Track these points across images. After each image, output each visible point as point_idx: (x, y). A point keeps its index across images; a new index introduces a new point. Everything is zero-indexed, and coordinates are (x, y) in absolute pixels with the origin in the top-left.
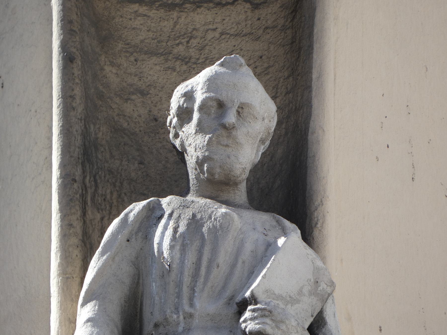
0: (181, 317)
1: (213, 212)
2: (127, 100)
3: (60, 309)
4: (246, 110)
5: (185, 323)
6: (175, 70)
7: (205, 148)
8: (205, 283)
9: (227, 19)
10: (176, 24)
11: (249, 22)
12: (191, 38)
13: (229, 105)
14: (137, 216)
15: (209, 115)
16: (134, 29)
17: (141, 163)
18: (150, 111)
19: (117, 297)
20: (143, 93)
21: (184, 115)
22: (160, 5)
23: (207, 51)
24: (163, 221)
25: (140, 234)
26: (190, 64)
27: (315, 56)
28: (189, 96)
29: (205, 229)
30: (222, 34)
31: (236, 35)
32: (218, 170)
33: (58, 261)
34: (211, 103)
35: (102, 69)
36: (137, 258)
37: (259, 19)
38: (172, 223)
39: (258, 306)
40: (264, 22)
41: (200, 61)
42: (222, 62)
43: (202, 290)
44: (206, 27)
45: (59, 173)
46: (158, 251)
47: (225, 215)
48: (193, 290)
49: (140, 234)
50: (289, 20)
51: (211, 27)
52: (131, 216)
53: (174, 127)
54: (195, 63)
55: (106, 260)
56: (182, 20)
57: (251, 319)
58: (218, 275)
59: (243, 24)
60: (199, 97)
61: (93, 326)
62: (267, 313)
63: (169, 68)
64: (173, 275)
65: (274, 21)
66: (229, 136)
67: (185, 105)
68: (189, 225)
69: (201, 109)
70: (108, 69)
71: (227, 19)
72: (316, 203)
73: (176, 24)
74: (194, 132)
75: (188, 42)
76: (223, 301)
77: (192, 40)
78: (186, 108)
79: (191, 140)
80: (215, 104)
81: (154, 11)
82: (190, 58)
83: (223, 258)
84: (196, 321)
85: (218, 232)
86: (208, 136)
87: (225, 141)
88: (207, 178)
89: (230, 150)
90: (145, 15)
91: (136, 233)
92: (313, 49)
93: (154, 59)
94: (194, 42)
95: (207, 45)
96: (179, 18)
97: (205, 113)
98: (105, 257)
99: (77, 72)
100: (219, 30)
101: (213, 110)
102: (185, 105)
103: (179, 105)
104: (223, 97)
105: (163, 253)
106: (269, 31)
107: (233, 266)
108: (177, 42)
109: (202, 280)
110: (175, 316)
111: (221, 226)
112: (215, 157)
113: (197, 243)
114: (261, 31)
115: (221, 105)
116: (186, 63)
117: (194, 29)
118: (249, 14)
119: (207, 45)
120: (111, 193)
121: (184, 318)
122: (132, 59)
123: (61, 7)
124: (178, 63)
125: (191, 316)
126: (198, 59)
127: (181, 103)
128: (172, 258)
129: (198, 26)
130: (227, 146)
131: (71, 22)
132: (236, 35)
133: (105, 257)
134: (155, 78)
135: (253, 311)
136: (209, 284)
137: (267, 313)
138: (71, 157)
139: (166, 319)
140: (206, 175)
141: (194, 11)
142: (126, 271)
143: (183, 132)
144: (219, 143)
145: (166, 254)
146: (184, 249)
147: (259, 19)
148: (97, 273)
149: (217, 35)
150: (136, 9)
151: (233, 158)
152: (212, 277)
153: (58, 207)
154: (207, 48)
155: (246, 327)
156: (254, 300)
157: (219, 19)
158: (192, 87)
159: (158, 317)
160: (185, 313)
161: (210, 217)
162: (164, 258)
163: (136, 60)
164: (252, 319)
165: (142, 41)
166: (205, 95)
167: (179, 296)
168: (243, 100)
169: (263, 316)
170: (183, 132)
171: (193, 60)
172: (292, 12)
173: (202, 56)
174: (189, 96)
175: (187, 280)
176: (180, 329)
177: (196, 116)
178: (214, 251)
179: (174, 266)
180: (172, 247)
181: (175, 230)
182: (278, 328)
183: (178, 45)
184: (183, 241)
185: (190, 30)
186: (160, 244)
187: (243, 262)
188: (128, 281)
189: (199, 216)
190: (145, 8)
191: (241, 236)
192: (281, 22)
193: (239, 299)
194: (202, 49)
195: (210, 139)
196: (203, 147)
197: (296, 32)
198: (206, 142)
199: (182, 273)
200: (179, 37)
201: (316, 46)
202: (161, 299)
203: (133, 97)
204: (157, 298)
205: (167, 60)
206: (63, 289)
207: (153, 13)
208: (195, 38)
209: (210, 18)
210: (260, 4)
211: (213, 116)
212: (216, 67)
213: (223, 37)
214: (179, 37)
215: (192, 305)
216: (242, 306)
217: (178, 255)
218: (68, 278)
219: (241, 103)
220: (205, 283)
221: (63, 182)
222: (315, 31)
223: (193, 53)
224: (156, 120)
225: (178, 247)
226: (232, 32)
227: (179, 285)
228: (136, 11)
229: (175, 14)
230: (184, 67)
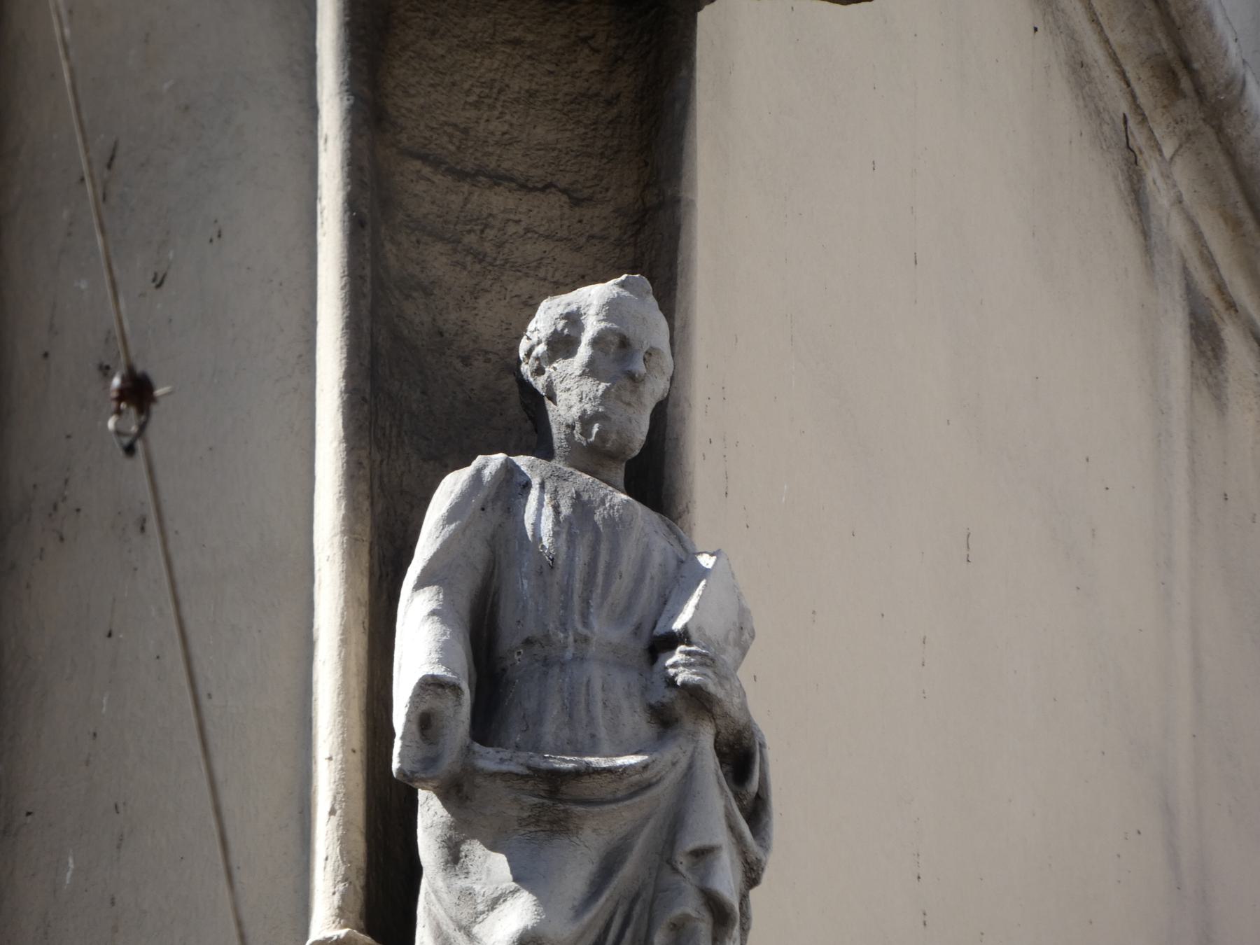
0: (571, 639)
1: (606, 495)
2: (408, 297)
3: (346, 582)
4: (654, 359)
5: (576, 648)
6: (465, 268)
7: (598, 401)
8: (604, 597)
9: (536, 210)
10: (466, 201)
11: (566, 223)
12: (486, 226)
13: (637, 347)
14: (495, 477)
15: (607, 354)
16: (416, 195)
17: (423, 393)
18: (434, 320)
19: (467, 585)
20: (427, 293)
21: (562, 345)
22: (447, 170)
23: (506, 250)
24: (534, 494)
25: (499, 504)
26: (484, 264)
27: (679, 295)
28: (574, 319)
29: (597, 518)
30: (527, 230)
31: (547, 237)
32: (614, 436)
33: (343, 512)
34: (611, 338)
35: (383, 246)
36: (493, 537)
37: (580, 221)
38: (547, 497)
39: (693, 648)
40: (588, 228)
41: (498, 262)
42: (623, 282)
43: (601, 606)
44: (507, 216)
45: (343, 384)
46: (533, 536)
47: (625, 504)
48: (586, 602)
49: (499, 504)
50: (629, 233)
51: (512, 216)
52: (487, 473)
53: (537, 358)
54: (491, 264)
55: (455, 530)
56: (475, 197)
57: (685, 665)
58: (621, 586)
59: (558, 223)
60: (592, 326)
61: (443, 622)
62: (708, 661)
63: (457, 263)
64: (559, 574)
65: (604, 229)
66: (635, 391)
67: (566, 331)
68: (573, 506)
69: (596, 342)
70: (388, 246)
71: (536, 210)
72: (680, 508)
73: (466, 201)
74: (578, 372)
75: (482, 231)
76: (628, 629)
77: (487, 231)
78: (568, 336)
79: (568, 383)
80: (616, 340)
81: (440, 177)
82: (485, 255)
83: (627, 565)
84: (592, 649)
85: (617, 525)
86: (603, 386)
87: (627, 396)
88: (590, 445)
89: (631, 410)
90: (429, 180)
91: (494, 501)
92: (675, 284)
93: (439, 247)
94: (490, 233)
95: (506, 241)
96: (471, 193)
97: (602, 350)
98: (453, 526)
99: (367, 241)
100: (523, 224)
101: (613, 349)
102: (566, 331)
103: (556, 330)
104: (629, 333)
105: (541, 539)
106: (595, 241)
107: (639, 580)
108: (468, 227)
109: (598, 591)
110: (562, 635)
111: (620, 518)
112: (613, 417)
113: (589, 537)
114: (583, 240)
115: (624, 343)
116: (480, 261)
117: (490, 215)
118: (566, 210)
119: (506, 241)
120: (391, 426)
121: (575, 641)
122: (414, 239)
123: (347, 145)
124: (469, 258)
125: (586, 640)
126: (495, 259)
127: (560, 327)
128: (557, 549)
129: (495, 212)
130: (629, 404)
131: (361, 169)
132: (547, 237)
133: (453, 526)
134: (440, 273)
135: (689, 653)
136: (610, 600)
137: (708, 661)
138: (361, 364)
139: (547, 636)
140: (592, 439)
141: (490, 188)
142: (479, 552)
143: (555, 369)
144: (619, 397)
145: (546, 541)
146: (572, 541)
147: (580, 221)
148: (441, 546)
149: (521, 232)
150: (418, 167)
151: (634, 423)
152: (613, 589)
153: (342, 434)
154: (508, 245)
155: (676, 675)
156: (683, 637)
157: (523, 208)
158: (579, 308)
159: (531, 629)
160: (576, 633)
161: (603, 502)
162: (543, 547)
163: (418, 242)
164: (687, 665)
165: (425, 216)
166: (603, 325)
167: (566, 606)
168: (654, 345)
169: (703, 664)
170: (555, 369)
171: (488, 259)
172: (634, 223)
173: (501, 257)
174: (574, 319)
175: (578, 586)
176: (569, 654)
177: (584, 352)
178: (615, 551)
179: (560, 562)
180: (556, 534)
181: (556, 509)
182: (721, 685)
183: (469, 232)
184: (570, 528)
185: (485, 215)
186: (536, 525)
187: (652, 578)
188: (481, 567)
189: (585, 497)
190: (428, 169)
191: (645, 539)
192: (615, 233)
193: (660, 630)
194: (500, 245)
195: (607, 391)
196: (595, 398)
197: (643, 254)
198: (600, 392)
199: (570, 574)
200: (470, 221)
201: (680, 281)
202: (537, 604)
203: (415, 294)
204: (531, 603)
205: (455, 251)
206: (350, 555)
207: (437, 178)
208: (493, 227)
209: (511, 204)
210: (583, 200)
211: (612, 357)
212: (617, 290)
213: (529, 235)
214: (470, 221)
215: (586, 624)
216: (671, 641)
217: (564, 548)
218: (356, 540)
219: (652, 348)
220: (604, 597)
221: (349, 398)
222: (680, 259)
223: (488, 247)
224: (441, 334)
225: (564, 536)
226: (541, 230)
227: (567, 591)
228: (419, 171)
229: (466, 187)
230: (477, 267)
